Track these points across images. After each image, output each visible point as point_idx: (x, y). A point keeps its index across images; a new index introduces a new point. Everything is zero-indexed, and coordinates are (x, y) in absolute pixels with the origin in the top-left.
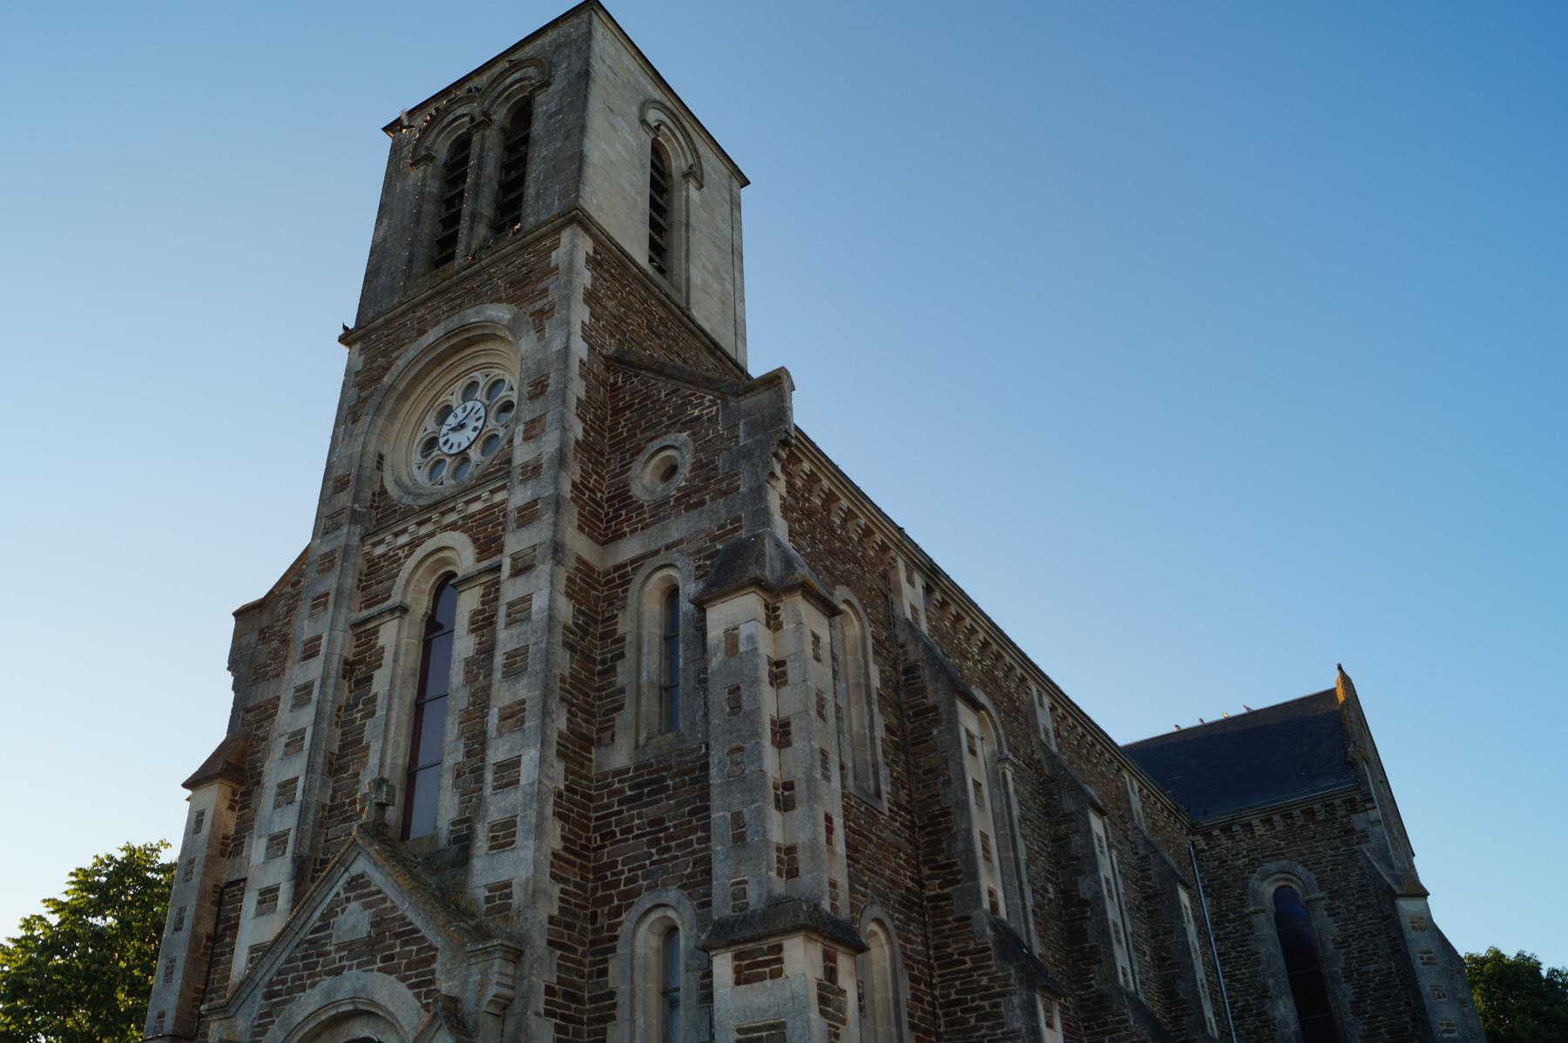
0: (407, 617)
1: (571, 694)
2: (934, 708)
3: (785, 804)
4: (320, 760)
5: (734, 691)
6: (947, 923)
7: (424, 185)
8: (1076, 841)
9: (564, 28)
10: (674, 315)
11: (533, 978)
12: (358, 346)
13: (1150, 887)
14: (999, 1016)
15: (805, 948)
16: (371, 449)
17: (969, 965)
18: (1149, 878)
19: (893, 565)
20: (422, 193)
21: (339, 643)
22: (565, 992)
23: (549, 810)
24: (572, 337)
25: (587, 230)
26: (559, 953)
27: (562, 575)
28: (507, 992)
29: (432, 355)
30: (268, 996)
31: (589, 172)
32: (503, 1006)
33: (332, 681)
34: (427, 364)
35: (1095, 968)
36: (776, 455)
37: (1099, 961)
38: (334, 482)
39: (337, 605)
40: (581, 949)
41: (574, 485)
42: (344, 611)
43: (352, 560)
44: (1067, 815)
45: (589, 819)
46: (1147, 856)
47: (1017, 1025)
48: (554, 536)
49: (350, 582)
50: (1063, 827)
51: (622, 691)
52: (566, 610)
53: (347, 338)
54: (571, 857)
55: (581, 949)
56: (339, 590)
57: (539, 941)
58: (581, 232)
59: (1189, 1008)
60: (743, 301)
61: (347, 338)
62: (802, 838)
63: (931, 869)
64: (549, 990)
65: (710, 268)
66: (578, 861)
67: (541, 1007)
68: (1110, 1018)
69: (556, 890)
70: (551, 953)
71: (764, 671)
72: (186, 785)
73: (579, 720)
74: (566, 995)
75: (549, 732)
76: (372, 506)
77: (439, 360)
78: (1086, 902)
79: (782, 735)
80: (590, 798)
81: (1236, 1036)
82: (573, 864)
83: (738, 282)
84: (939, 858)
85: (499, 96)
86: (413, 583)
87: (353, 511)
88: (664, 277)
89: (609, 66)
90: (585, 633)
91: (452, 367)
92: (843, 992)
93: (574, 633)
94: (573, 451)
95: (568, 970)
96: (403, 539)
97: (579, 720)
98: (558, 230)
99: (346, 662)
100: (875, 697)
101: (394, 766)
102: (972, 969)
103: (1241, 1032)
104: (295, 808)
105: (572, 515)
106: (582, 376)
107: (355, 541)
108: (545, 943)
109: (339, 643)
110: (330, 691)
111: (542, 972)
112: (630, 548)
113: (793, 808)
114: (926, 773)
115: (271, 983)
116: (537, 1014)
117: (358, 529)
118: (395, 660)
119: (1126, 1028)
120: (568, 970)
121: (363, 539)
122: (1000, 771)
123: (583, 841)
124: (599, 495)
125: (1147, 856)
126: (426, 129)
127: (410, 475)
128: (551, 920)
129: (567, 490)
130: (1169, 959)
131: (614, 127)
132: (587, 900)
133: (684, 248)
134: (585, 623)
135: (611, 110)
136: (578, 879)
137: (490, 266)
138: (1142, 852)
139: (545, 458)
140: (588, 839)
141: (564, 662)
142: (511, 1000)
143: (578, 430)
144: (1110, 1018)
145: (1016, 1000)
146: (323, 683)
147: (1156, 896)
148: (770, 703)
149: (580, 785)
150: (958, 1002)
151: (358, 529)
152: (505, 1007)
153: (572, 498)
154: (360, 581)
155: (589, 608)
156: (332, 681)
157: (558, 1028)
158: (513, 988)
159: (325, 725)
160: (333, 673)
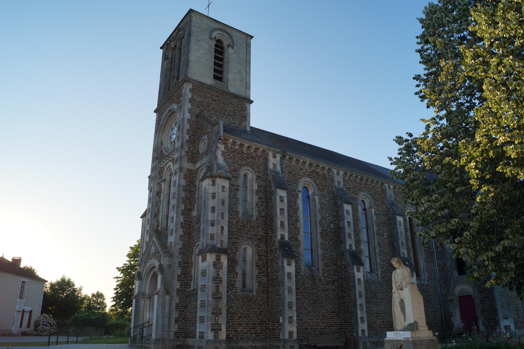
0: (166, 182)
1: (185, 201)
2: (273, 191)
3: (212, 225)
4: (153, 214)
5: (205, 201)
6: (272, 242)
7: (167, 66)
8: (340, 212)
9: (185, 19)
10: (220, 93)
11: (175, 261)
12: (157, 113)
13: (390, 216)
14: (278, 263)
15: (209, 255)
16: (159, 141)
17: (274, 252)
18: (390, 214)
19: (268, 154)
20: (166, 69)
21: (155, 188)
22: (184, 262)
23: (179, 227)
24: (185, 114)
25: (189, 82)
26: (182, 255)
27: (182, 174)
28: (170, 263)
29: (167, 116)
30: (144, 263)
31: (191, 64)
32: (170, 266)
33: (154, 197)
34: (167, 118)
35: (342, 245)
36: (218, 142)
37: (343, 243)
38: (155, 150)
39: (154, 180)
40: (188, 254)
41: (186, 152)
42: (156, 181)
43: (157, 169)
44: (339, 205)
45: (191, 227)
46: (389, 208)
47: (280, 265)
48: (180, 166)
49: (157, 174)
50: (338, 209)
51: (196, 198)
52: (183, 182)
53: (155, 111)
54: (186, 235)
55: (188, 254)
56: (155, 176)
57: (177, 253)
58: (188, 83)
59: (397, 250)
60: (250, 76)
61: (155, 111)
62: (215, 232)
63: (270, 230)
64: (179, 262)
65: (236, 71)
66: (188, 236)
67: (177, 266)
68: (344, 257)
69: (181, 243)
70: (180, 255)
71: (210, 196)
72: (141, 218)
73: (188, 206)
74: (184, 263)
75: (179, 210)
76: (161, 155)
77: (169, 117)
78: (341, 228)
79: (213, 209)
80: (191, 222)
81: (436, 253)
82: (186, 237)
83: (248, 71)
84: (272, 227)
85: (178, 39)
86: (166, 174)
87: (157, 157)
88: (222, 81)
89: (198, 27)
90: (189, 185)
91: (172, 118)
92: (408, 237)
93: (186, 187)
94: (185, 143)
95: (185, 258)
96: (165, 163)
97: (188, 206)
98: (183, 84)
99: (157, 192)
100: (255, 192)
101: (164, 215)
102: (275, 253)
103: (437, 252)
104: (149, 224)
105: (186, 159)
106: (188, 123)
107: (157, 164)
108: (178, 253)
109: (155, 188)
110: (154, 199)
111: (177, 259)
112: (198, 165)
113: (214, 226)
114: (271, 207)
115: (145, 261)
116: (176, 267)
117: (158, 161)
118: (164, 192)
119: (347, 260)
120: (185, 258)
121: (159, 163)
122: (314, 198)
123: (189, 232)
124: (194, 151)
125: (389, 208)
126: (166, 49)
127: (167, 146)
128: (180, 249)
129: (184, 153)
130: (393, 236)
131: (200, 46)
132: (190, 243)
133: (227, 70)
134: (190, 183)
135: (198, 41)
136: (188, 240)
137: (174, 93)
138: (388, 207)
139: (179, 146)
140: (190, 231)
141: (183, 194)
142: (171, 265)
143: (187, 137)
144: (344, 257)
145: (280, 260)
146: (153, 198)
147: (391, 219)
148: (211, 203)
149: (188, 220)
150: (273, 260)
151: (158, 161)
152: (171, 266)
153: (185, 155)
154: (159, 173)
155: (191, 180)
156: (154, 197)
157: (182, 269)
158: (172, 262)
159: (154, 207)
160: (154, 195)
